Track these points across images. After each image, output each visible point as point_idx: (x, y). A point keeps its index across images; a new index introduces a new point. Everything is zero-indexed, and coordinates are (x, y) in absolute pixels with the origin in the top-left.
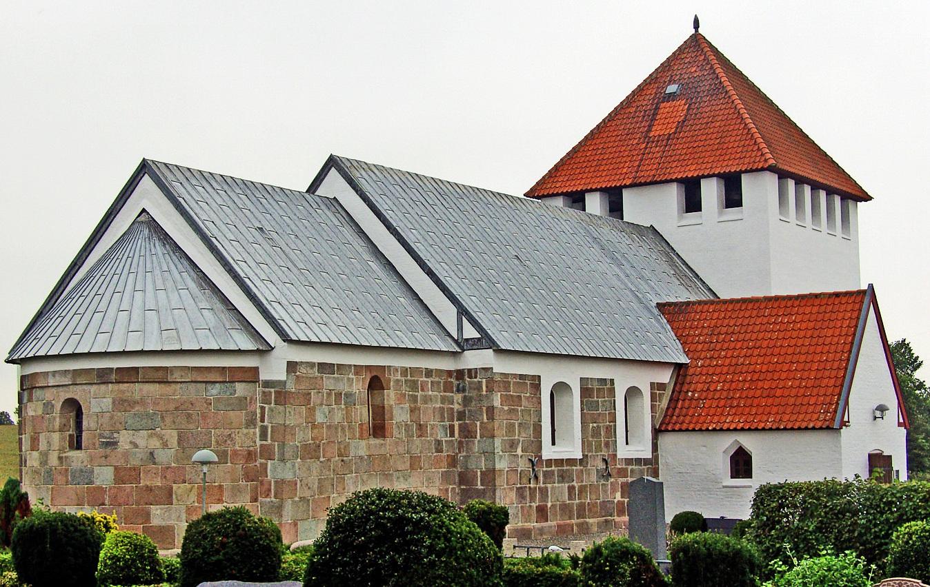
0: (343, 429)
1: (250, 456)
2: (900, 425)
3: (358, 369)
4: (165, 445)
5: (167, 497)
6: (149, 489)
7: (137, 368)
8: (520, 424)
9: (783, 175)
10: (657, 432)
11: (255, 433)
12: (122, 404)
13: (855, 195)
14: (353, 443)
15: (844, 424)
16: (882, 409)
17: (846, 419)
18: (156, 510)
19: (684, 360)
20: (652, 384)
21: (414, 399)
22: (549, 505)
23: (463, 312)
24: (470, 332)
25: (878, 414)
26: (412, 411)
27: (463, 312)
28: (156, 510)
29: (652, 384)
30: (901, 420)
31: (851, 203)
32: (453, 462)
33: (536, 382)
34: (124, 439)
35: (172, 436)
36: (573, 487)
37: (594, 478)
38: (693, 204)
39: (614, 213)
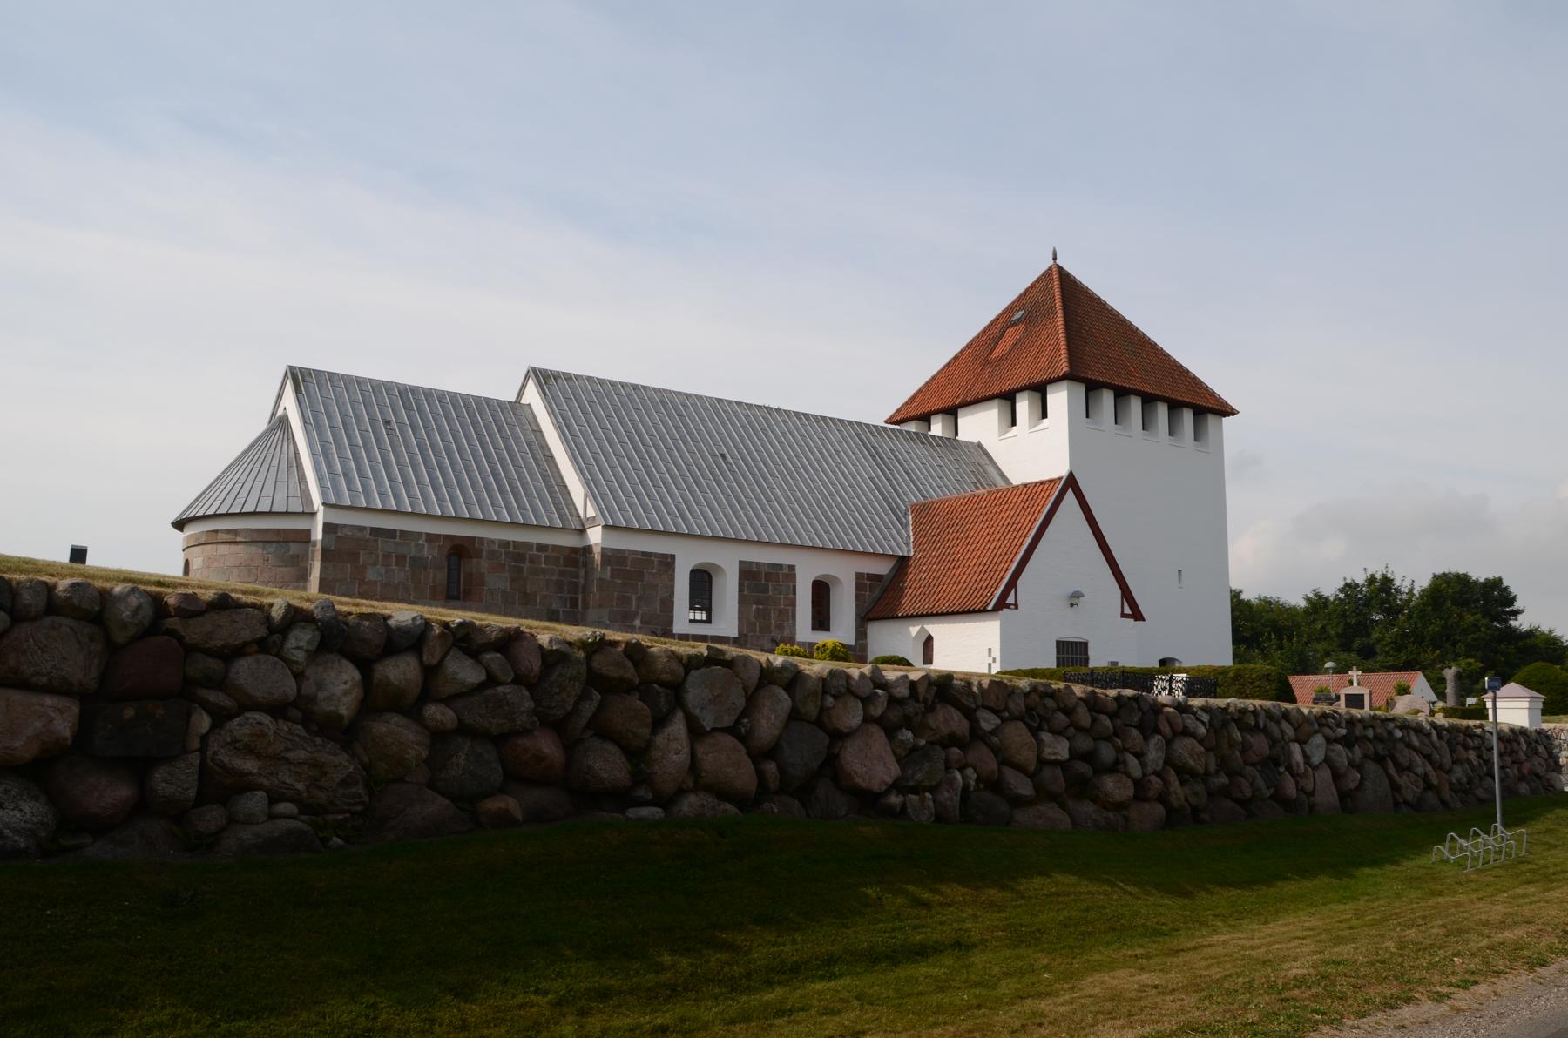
3: (431, 538)
8: (639, 599)
13: (1199, 406)
17: (1011, 600)
20: (859, 576)
21: (520, 570)
26: (513, 580)
29: (859, 576)
31: (1211, 419)
33: (668, 562)
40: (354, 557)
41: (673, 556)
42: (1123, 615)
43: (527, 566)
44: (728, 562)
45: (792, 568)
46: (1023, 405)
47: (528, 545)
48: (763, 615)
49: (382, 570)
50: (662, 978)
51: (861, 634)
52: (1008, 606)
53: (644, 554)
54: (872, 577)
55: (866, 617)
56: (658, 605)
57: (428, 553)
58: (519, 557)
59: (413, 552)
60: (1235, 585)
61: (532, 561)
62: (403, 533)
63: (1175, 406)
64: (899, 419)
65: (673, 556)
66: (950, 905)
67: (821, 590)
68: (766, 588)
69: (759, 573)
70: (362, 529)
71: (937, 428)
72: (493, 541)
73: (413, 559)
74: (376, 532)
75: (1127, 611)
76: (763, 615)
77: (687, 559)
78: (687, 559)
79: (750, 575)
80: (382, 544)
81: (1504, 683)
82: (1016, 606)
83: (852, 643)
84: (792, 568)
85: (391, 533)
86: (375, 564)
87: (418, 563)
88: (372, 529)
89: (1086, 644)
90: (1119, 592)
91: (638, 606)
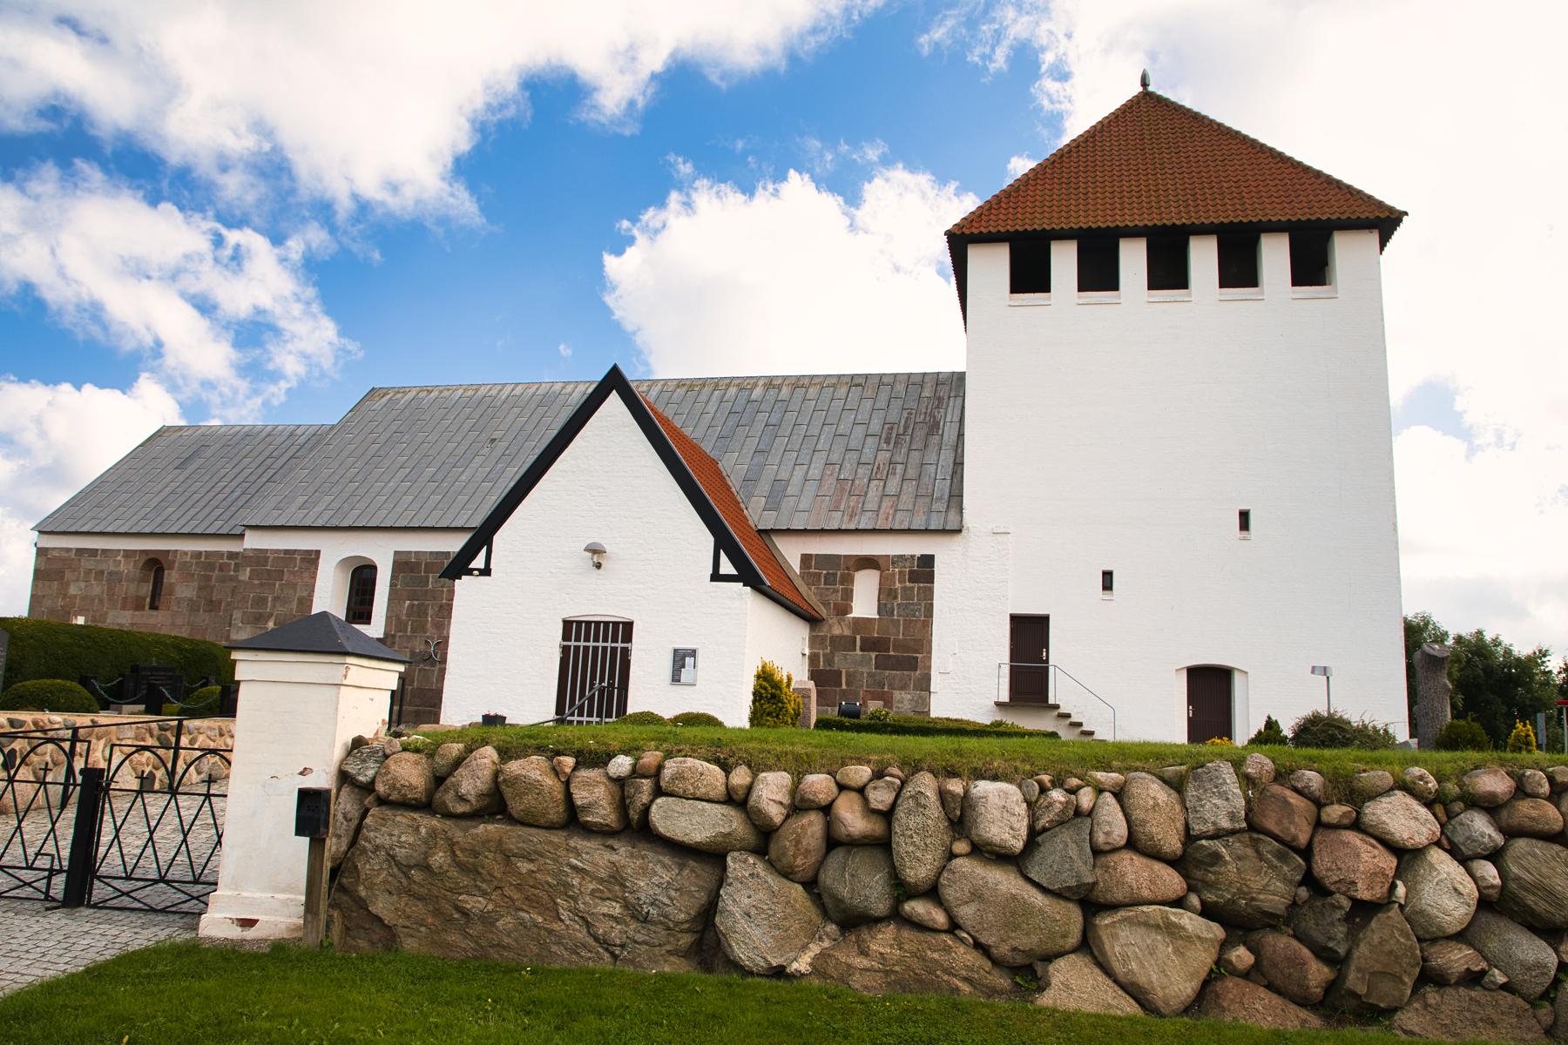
0: (101, 601)
3: (128, 554)
8: (275, 599)
17: (479, 562)
21: (208, 578)
26: (200, 588)
42: (716, 577)
47: (219, 554)
48: (419, 613)
49: (82, 585)
53: (286, 552)
56: (294, 605)
57: (125, 567)
58: (210, 566)
59: (112, 568)
60: (1411, 610)
61: (221, 570)
62: (104, 551)
66: (393, 857)
69: (418, 564)
72: (186, 553)
73: (110, 574)
74: (80, 551)
75: (727, 567)
76: (419, 613)
80: (87, 564)
81: (714, 925)
82: (486, 571)
87: (114, 577)
88: (78, 550)
90: (709, 540)
91: (274, 606)
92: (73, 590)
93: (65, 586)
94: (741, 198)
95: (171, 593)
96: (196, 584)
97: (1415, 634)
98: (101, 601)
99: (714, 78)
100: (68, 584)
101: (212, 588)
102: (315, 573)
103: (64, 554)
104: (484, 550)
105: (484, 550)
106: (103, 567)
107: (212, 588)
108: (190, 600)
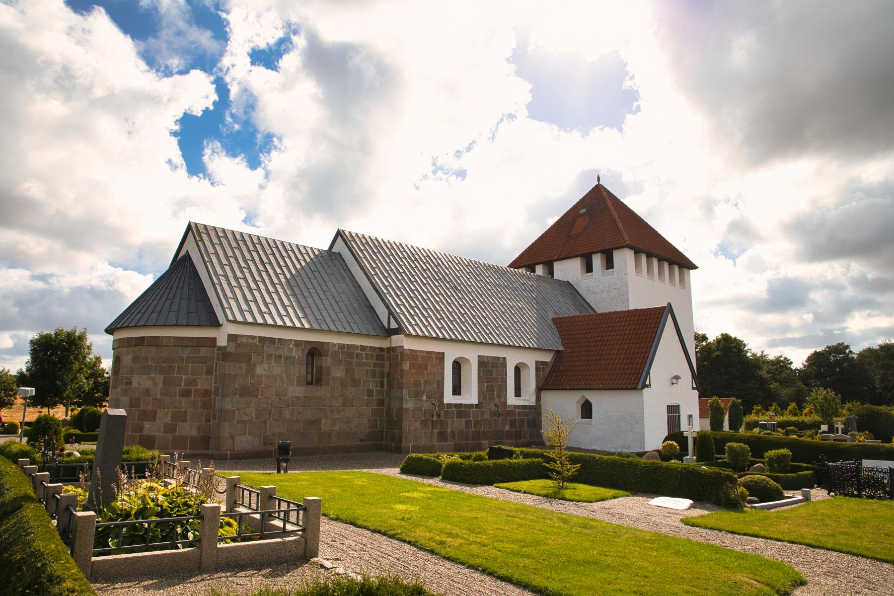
0: (282, 379)
1: (207, 392)
2: (693, 388)
3: (298, 343)
4: (155, 384)
5: (153, 417)
6: (145, 412)
7: (143, 338)
8: (425, 382)
9: (637, 252)
10: (540, 389)
11: (211, 379)
12: (136, 359)
13: (684, 264)
14: (291, 389)
15: (645, 386)
16: (677, 378)
17: (647, 383)
18: (147, 425)
19: (561, 348)
20: (537, 362)
21: (350, 363)
22: (449, 431)
23: (391, 313)
24: (394, 325)
25: (674, 381)
26: (347, 370)
27: (391, 313)
28: (147, 425)
29: (537, 362)
30: (694, 386)
31: (686, 270)
32: (381, 403)
33: (441, 357)
34: (136, 380)
35: (160, 379)
36: (470, 421)
37: (487, 416)
38: (589, 269)
39: (76, 212)
40: (248, 358)
41: (443, 353)
43: (355, 360)
44: (472, 355)
45: (504, 359)
46: (597, 261)
47: (355, 347)
49: (266, 366)
50: (88, 457)
51: (538, 399)
52: (647, 386)
53: (428, 352)
54: (543, 363)
55: (541, 388)
59: (287, 354)
61: (357, 358)
62: (280, 340)
63: (671, 263)
64: (515, 264)
65: (443, 353)
67: (457, 366)
68: (491, 370)
69: (488, 363)
70: (254, 338)
71: (540, 270)
72: (334, 345)
73: (286, 358)
74: (262, 339)
76: (490, 389)
77: (451, 354)
78: (451, 354)
79: (483, 363)
80: (268, 349)
83: (218, 344)
84: (504, 359)
85: (272, 341)
86: (262, 363)
88: (260, 338)
89: (679, 406)
92: (259, 370)
93: (252, 367)
94: (527, 102)
95: (329, 373)
96: (343, 367)
97: (621, 130)
98: (282, 379)
99: (749, 354)
100: (255, 365)
101: (354, 370)
102: (443, 366)
103: (251, 341)
104: (180, 257)
105: (180, 257)
106: (280, 352)
107: (354, 370)
108: (341, 378)
